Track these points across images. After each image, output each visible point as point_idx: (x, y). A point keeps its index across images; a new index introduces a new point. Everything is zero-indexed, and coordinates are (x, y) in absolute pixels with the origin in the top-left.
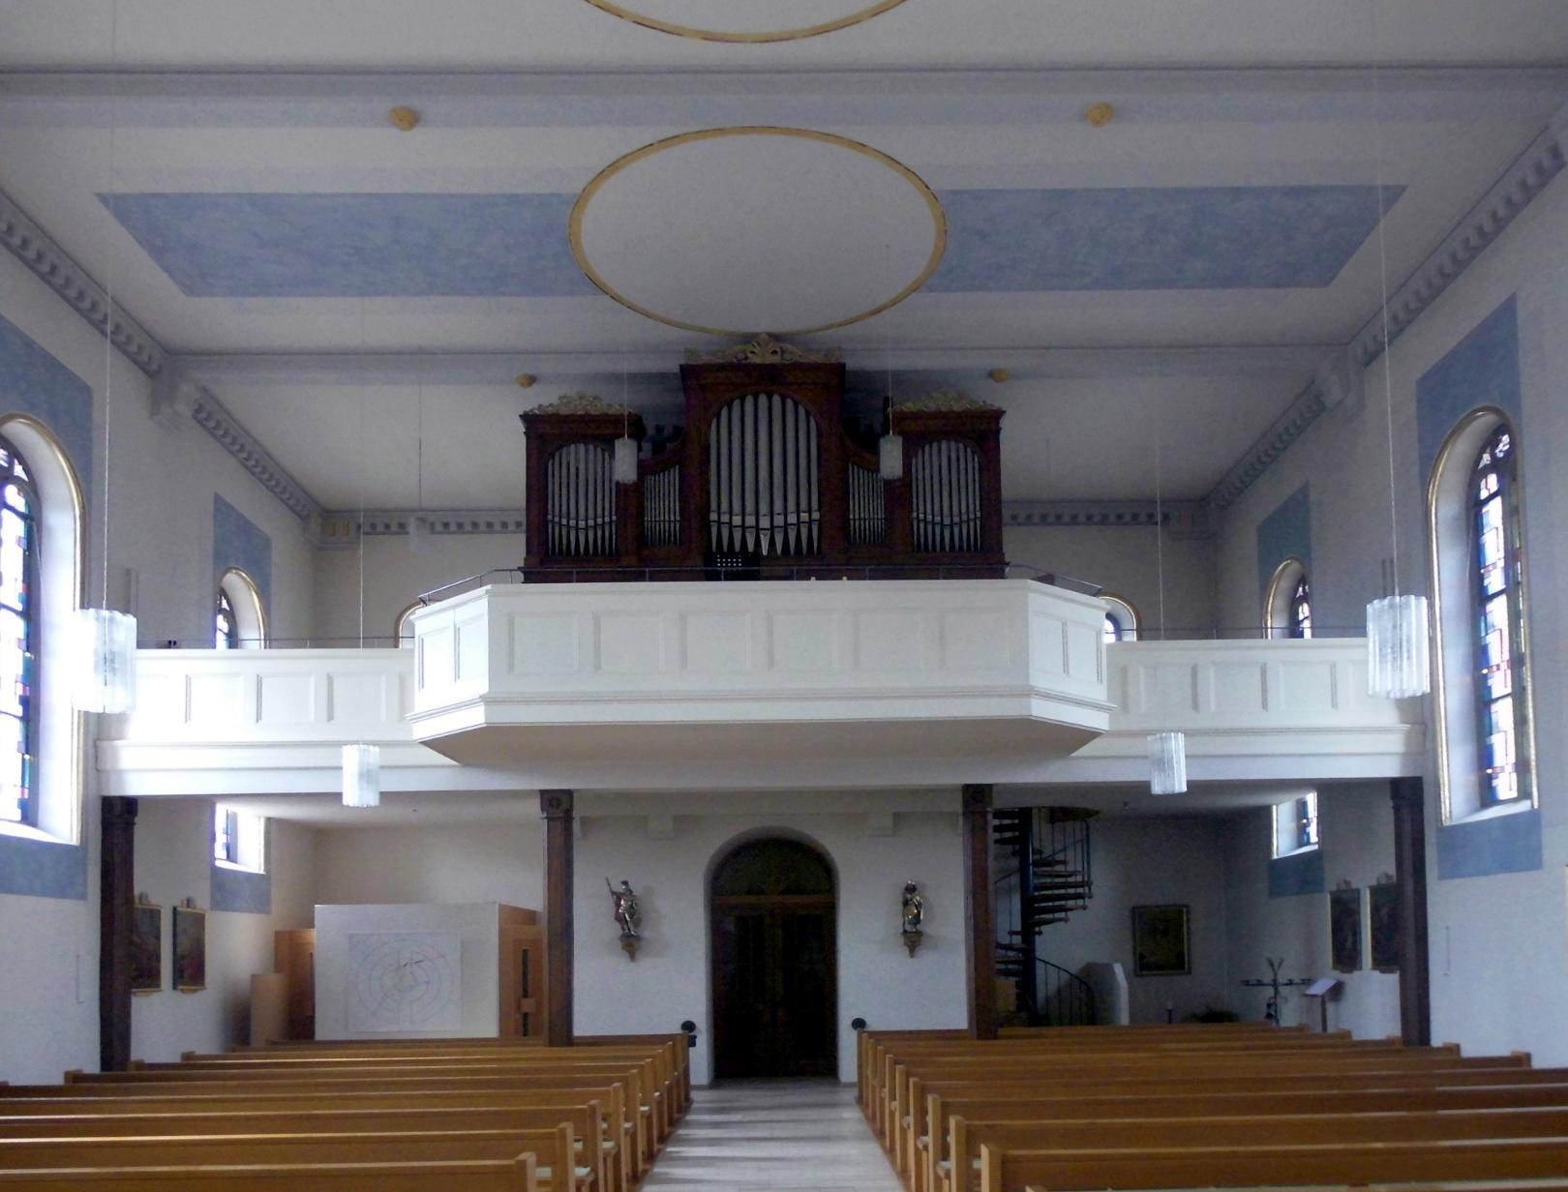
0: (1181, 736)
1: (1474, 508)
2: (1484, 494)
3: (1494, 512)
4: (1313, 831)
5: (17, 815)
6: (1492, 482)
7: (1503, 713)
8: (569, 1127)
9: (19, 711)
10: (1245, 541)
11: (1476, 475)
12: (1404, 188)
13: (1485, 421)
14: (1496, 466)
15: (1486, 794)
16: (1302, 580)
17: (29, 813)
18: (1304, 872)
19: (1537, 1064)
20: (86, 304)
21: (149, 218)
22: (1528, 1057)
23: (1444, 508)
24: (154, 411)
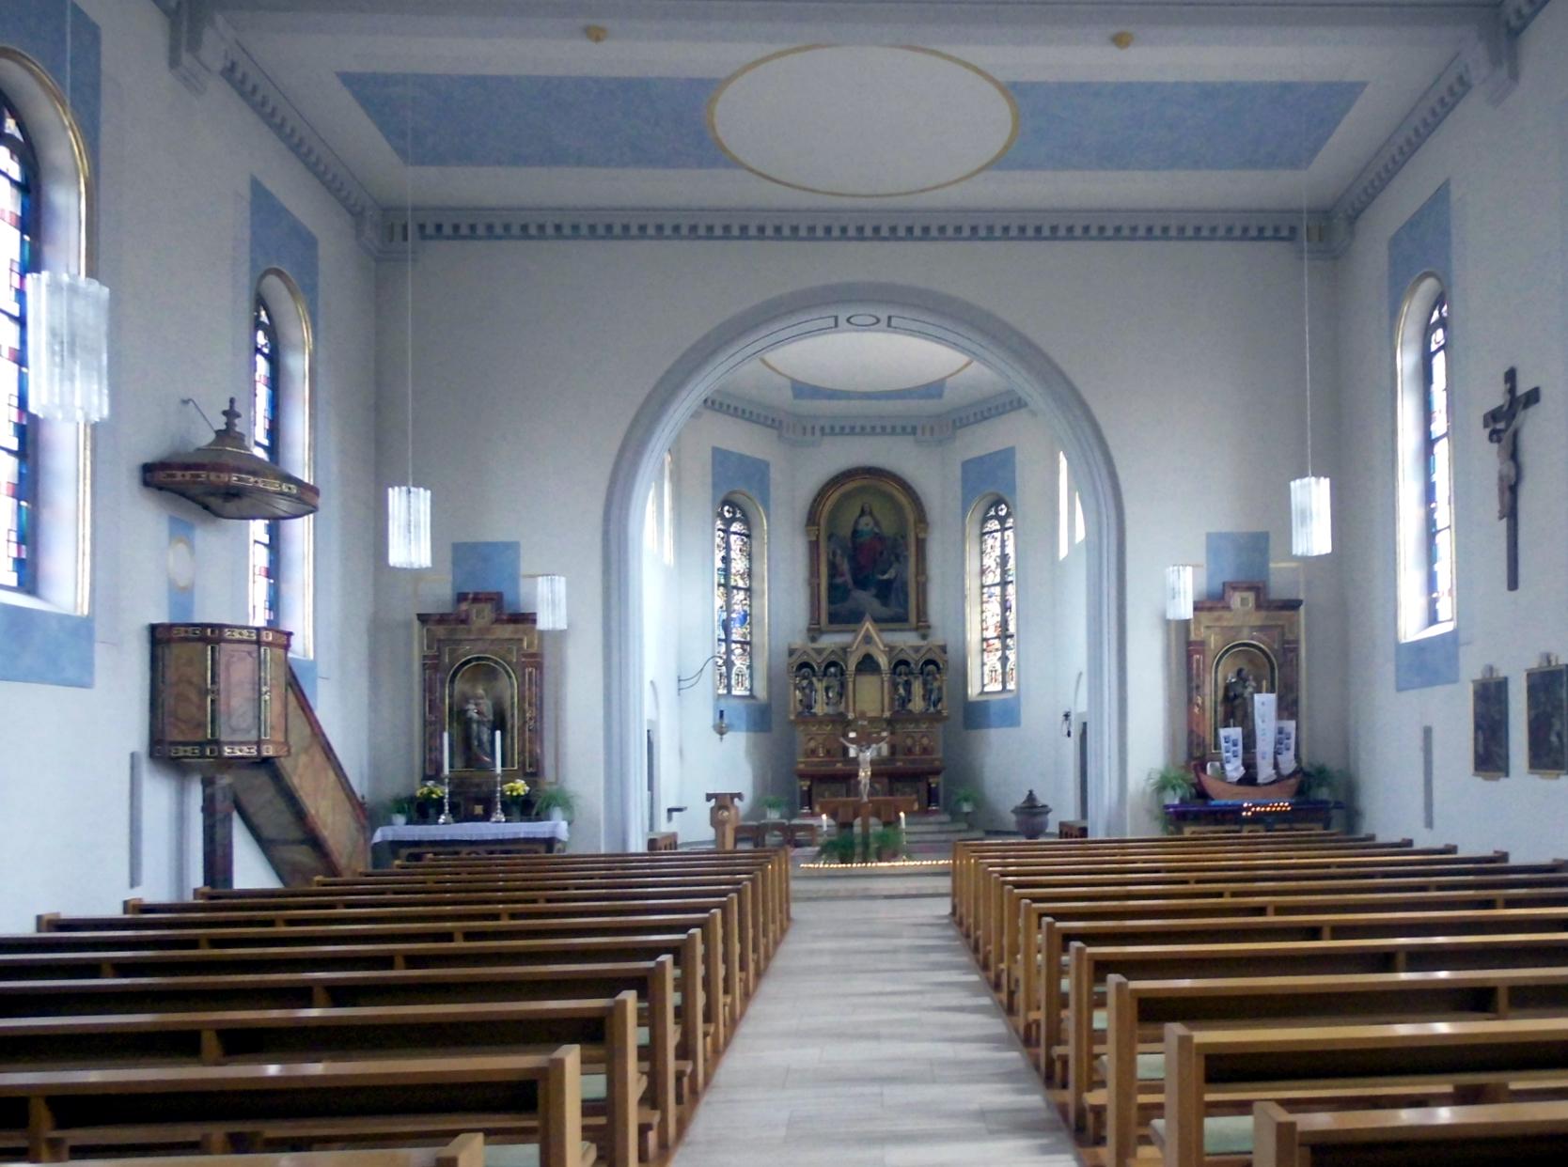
0: (1189, 569)
1: (1427, 358)
2: (1434, 347)
3: (1439, 363)
4: (1446, 608)
5: (12, 579)
6: (1439, 336)
7: (1445, 542)
8: (667, 958)
9: (14, 444)
10: (1372, 252)
11: (1428, 331)
12: (1364, 84)
13: (1429, 286)
14: (1443, 323)
15: (1433, 619)
16: (1439, 301)
17: (28, 574)
18: (1426, 663)
19: (1514, 861)
20: (258, 98)
21: (371, 91)
22: (1504, 857)
23: (1406, 361)
24: (174, 62)
